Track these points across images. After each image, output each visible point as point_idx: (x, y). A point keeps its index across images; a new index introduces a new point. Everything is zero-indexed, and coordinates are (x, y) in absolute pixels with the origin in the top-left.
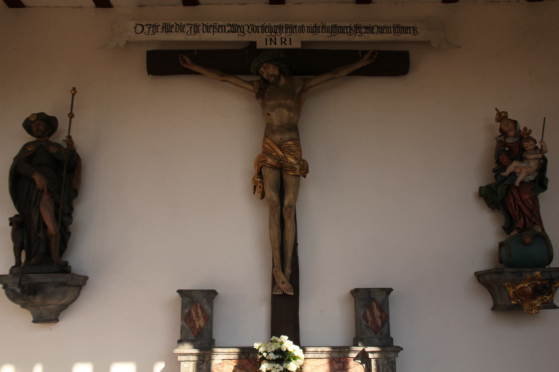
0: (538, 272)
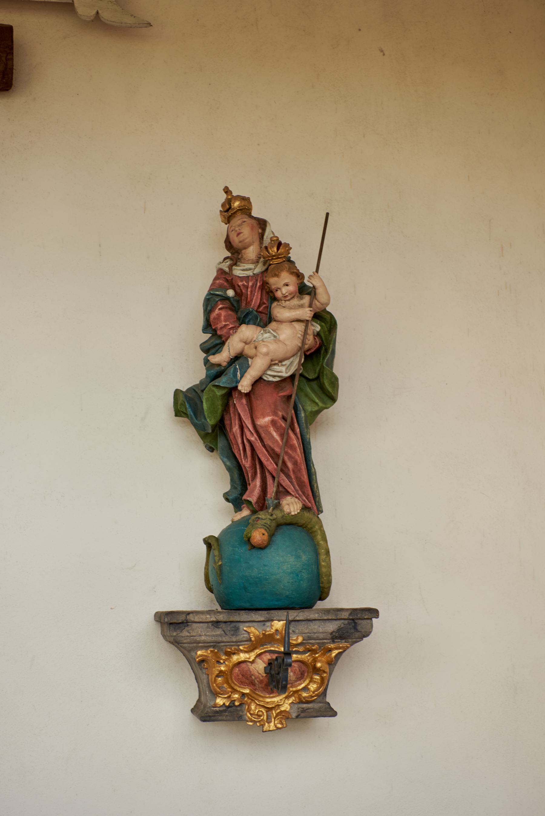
0: (279, 621)
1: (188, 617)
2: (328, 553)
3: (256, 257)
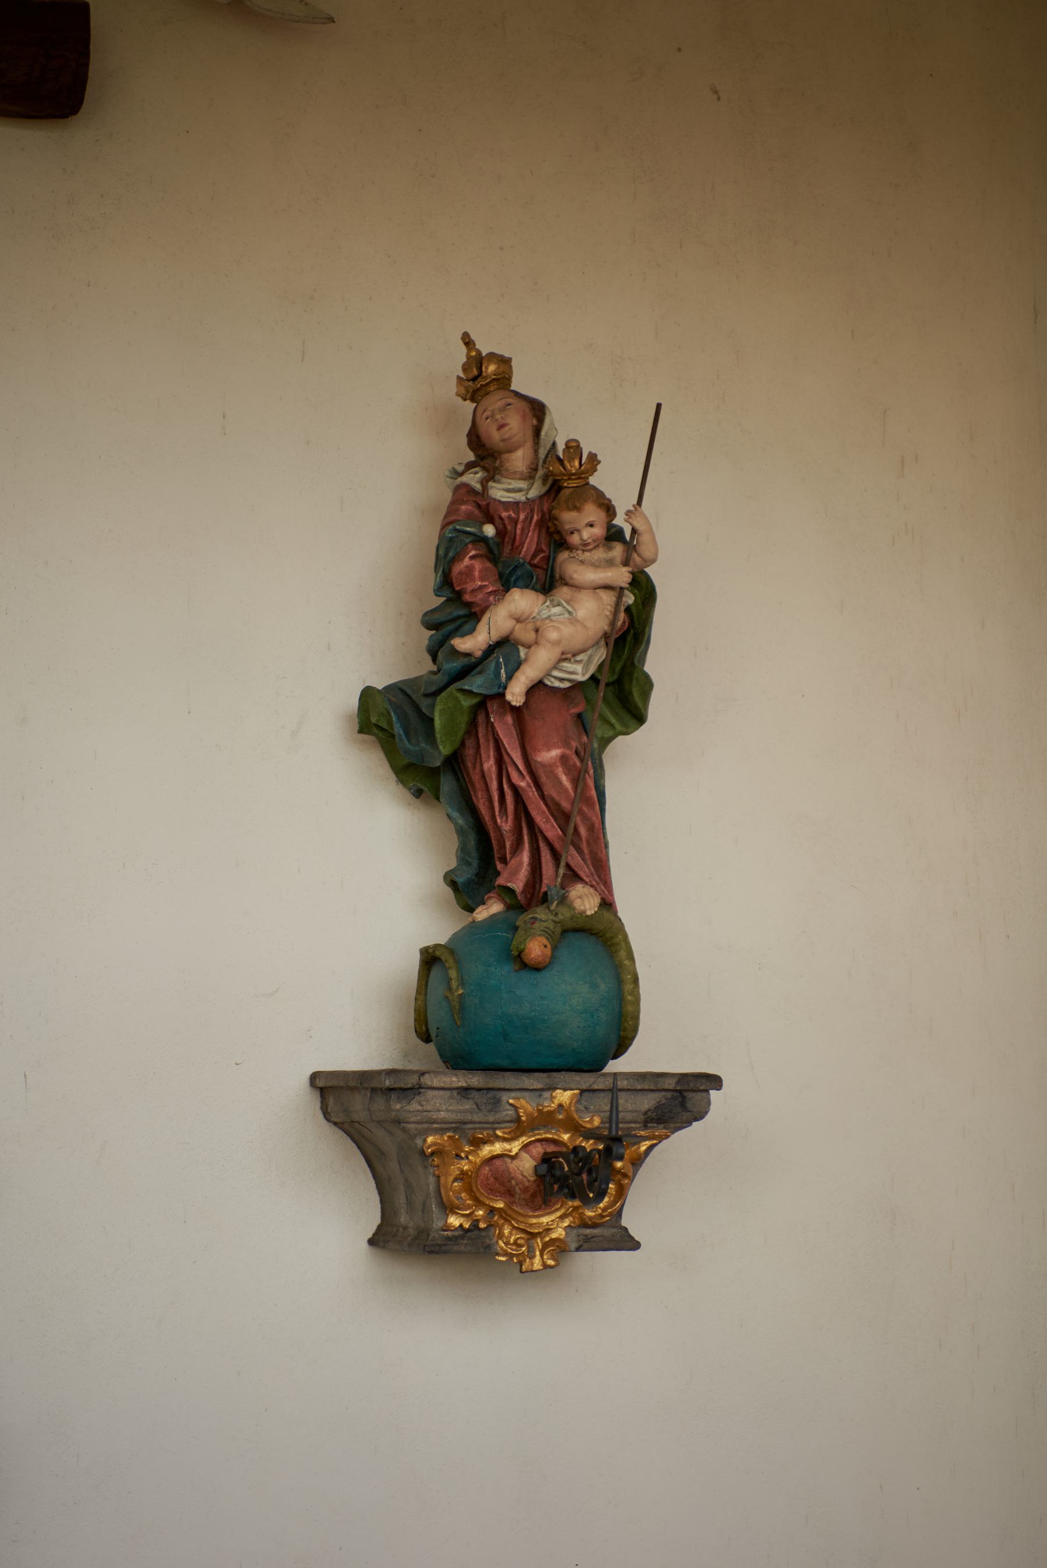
0: (565, 1090)
1: (421, 1079)
2: (636, 980)
3: (526, 468)
